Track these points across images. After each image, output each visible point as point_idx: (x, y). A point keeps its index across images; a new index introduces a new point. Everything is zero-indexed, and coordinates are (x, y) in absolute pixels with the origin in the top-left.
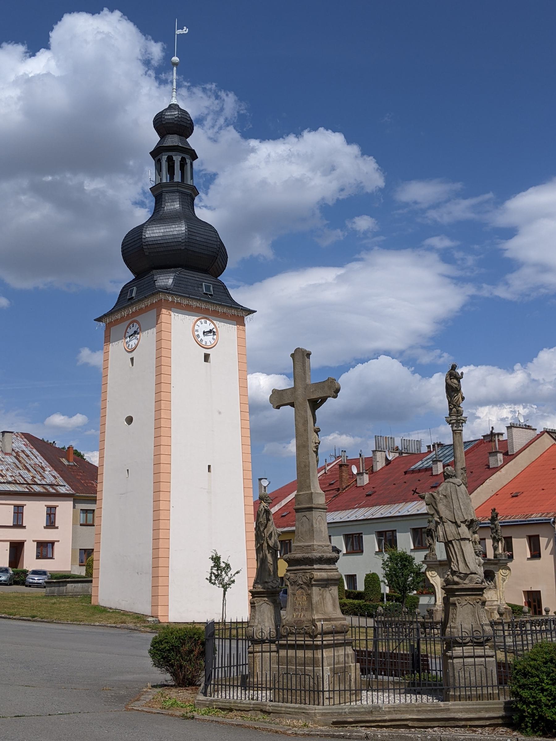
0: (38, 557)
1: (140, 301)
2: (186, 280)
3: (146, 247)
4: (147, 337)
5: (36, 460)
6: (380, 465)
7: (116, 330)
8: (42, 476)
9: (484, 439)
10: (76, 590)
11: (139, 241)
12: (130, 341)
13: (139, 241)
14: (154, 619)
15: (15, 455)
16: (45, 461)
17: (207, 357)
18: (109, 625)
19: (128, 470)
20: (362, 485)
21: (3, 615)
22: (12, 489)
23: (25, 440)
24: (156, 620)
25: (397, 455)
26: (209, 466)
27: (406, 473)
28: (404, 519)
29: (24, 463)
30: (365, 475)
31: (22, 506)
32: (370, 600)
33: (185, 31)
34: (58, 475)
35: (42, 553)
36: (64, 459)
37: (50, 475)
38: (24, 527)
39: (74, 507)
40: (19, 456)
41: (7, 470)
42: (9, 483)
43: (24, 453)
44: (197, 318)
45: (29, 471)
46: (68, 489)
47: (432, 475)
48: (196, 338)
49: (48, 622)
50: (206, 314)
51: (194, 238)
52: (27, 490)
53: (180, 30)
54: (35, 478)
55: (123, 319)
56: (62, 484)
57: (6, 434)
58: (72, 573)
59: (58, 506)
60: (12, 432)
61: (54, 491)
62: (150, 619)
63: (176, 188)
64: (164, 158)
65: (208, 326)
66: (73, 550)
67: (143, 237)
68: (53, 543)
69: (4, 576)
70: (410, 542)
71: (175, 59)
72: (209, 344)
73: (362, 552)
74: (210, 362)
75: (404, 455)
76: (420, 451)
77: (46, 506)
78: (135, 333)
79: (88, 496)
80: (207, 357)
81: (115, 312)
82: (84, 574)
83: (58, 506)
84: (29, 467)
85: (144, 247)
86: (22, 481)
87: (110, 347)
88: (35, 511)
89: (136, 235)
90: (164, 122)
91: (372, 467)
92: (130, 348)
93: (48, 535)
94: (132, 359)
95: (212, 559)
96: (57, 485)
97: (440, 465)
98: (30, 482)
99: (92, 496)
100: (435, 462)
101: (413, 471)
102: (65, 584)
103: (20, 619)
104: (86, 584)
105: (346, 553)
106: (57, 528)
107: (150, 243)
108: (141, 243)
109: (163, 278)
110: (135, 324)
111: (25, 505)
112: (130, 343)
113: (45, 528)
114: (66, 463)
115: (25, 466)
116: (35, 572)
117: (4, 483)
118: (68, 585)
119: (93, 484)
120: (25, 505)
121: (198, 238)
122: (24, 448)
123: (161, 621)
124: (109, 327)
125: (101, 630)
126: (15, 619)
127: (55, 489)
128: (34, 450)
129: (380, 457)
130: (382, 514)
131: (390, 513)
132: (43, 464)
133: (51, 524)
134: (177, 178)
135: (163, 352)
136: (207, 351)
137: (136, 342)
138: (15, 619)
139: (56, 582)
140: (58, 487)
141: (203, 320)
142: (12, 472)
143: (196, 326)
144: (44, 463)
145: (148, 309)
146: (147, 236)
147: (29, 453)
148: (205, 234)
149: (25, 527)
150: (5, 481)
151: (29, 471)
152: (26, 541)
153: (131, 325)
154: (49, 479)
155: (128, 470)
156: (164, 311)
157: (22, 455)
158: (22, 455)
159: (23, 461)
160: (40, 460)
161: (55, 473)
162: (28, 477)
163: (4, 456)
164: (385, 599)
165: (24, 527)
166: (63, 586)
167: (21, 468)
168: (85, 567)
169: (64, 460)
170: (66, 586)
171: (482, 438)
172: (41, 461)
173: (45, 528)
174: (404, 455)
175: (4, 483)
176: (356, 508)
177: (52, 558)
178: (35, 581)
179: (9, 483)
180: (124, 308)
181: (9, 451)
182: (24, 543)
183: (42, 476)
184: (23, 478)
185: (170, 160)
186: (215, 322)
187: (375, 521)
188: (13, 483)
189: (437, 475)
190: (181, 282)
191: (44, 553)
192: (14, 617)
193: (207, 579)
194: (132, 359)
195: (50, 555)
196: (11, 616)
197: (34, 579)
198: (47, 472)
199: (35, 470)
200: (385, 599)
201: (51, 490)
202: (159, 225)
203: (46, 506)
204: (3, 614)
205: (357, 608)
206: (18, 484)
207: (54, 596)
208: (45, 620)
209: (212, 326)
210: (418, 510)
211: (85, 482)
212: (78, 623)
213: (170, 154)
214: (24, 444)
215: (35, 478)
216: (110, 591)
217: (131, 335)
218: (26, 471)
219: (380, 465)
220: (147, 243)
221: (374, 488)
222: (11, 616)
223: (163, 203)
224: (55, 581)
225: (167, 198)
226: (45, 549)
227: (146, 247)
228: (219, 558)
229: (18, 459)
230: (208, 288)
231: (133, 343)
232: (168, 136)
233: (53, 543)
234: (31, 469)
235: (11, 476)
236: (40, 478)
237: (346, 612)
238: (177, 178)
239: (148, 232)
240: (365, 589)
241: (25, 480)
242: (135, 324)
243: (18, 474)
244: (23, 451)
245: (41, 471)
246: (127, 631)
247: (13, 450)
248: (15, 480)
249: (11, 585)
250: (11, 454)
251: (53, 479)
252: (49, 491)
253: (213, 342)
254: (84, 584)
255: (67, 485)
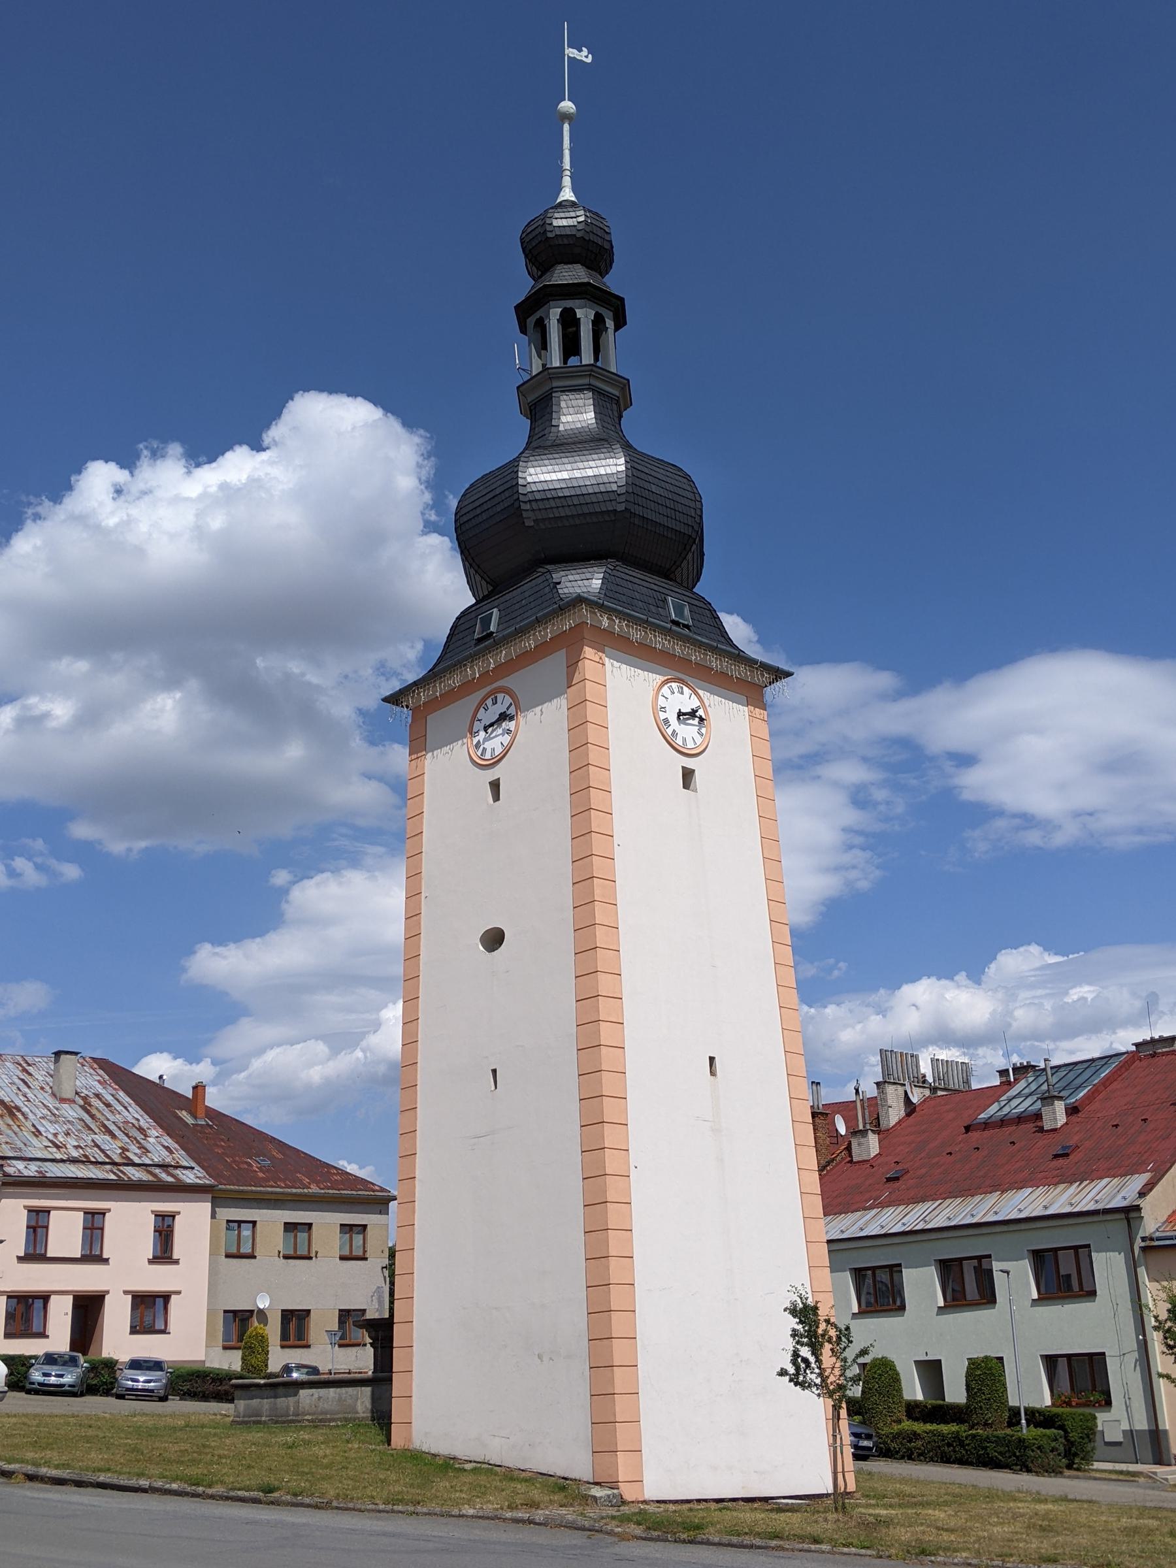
0: (134, 1331)
1: (506, 640)
2: (630, 585)
3: (528, 507)
4: (541, 728)
5: (126, 1113)
6: (894, 1114)
7: (434, 721)
8: (141, 1147)
9: (1138, 1051)
10: (323, 1406)
11: (507, 494)
12: (485, 740)
13: (507, 494)
14: (609, 1492)
15: (82, 1103)
16: (146, 1117)
17: (688, 776)
18: (509, 1515)
19: (494, 1071)
20: (866, 1158)
21: (174, 1486)
22: (80, 1175)
23: (101, 1072)
24: (614, 1496)
25: (927, 1093)
26: (712, 1059)
27: (968, 1129)
28: (1012, 1227)
29: (102, 1118)
30: (871, 1136)
31: (103, 1213)
32: (986, 1424)
33: (584, 56)
34: (176, 1146)
35: (142, 1322)
36: (184, 1113)
37: (159, 1146)
38: (106, 1261)
39: (213, 1216)
40: (90, 1105)
41: (67, 1134)
42: (74, 1161)
43: (100, 1100)
44: (663, 678)
45: (113, 1136)
46: (199, 1175)
47: (1041, 1130)
48: (662, 724)
49: (316, 1507)
50: (682, 670)
51: (646, 485)
52: (113, 1177)
53: (575, 51)
54: (128, 1150)
55: (467, 688)
56: (185, 1164)
57: (63, 1057)
58: (207, 1365)
59: (179, 1213)
60: (76, 1054)
61: (170, 1179)
62: (597, 1492)
63: (586, 381)
64: (554, 314)
65: (688, 701)
66: (211, 1313)
67: (521, 482)
68: (166, 1297)
69: (71, 1372)
70: (1029, 1284)
71: (567, 105)
72: (690, 745)
73: (994, 1302)
74: (695, 791)
75: (940, 1093)
76: (970, 1086)
77: (152, 1212)
78: (504, 717)
79: (242, 1191)
80: (688, 776)
81: (444, 670)
82: (237, 1366)
83: (179, 1213)
84: (113, 1128)
85: (523, 506)
86: (101, 1158)
87: (426, 762)
88: (129, 1222)
89: (499, 483)
90: (550, 235)
91: (878, 1118)
92: (488, 756)
93: (157, 1279)
94: (495, 786)
95: (793, 1311)
96: (176, 1167)
97: (1060, 1106)
98: (117, 1159)
99: (252, 1192)
100: (1048, 1099)
101: (986, 1125)
102: (291, 1390)
103: (227, 1498)
104: (350, 1390)
105: (860, 1313)
106: (177, 1262)
107: (538, 497)
108: (515, 497)
109: (577, 577)
110: (500, 696)
111: (109, 1210)
112: (488, 745)
113: (150, 1262)
114: (190, 1120)
115: (105, 1126)
116: (136, 1365)
117: (62, 1161)
118: (302, 1392)
119: (250, 1165)
120: (109, 1210)
121: (654, 488)
122: (100, 1089)
123: (628, 1497)
124: (420, 715)
125: (479, 1532)
126: (212, 1497)
127: (173, 1176)
128: (121, 1093)
129: (894, 1095)
130: (949, 1218)
131: (973, 1216)
132: (142, 1123)
133: (164, 1253)
134: (587, 357)
135: (591, 755)
136: (690, 763)
137: (506, 739)
138: (212, 1497)
139: (265, 1385)
140: (178, 1172)
141: (674, 685)
142: (79, 1138)
143: (660, 698)
144: (145, 1121)
145: (544, 650)
146: (529, 479)
147: (110, 1099)
148: (669, 480)
149: (106, 1261)
150: (65, 1157)
151: (113, 1136)
152: (108, 1292)
153: (489, 702)
154: (158, 1154)
155: (494, 1071)
156: (588, 652)
157: (95, 1102)
158: (95, 1102)
159: (98, 1115)
160: (135, 1114)
161: (168, 1141)
162: (113, 1148)
163: (58, 1105)
164: (1023, 1421)
165: (106, 1261)
166: (286, 1397)
167: (97, 1130)
168: (239, 1353)
169: (184, 1115)
170: (296, 1394)
171: (1134, 1048)
172: (136, 1116)
173: (150, 1262)
174: (940, 1093)
175: (62, 1161)
176: (871, 1208)
177: (164, 1332)
178: (140, 1385)
179: (74, 1161)
180: (473, 658)
181: (69, 1094)
182: (103, 1297)
183: (141, 1147)
184: (102, 1151)
185: (569, 322)
186: (700, 692)
187: (934, 1236)
188: (83, 1162)
189: (1055, 1130)
190: (620, 589)
191: (148, 1320)
192: (210, 1491)
193: (783, 1373)
194: (495, 786)
195: (159, 1325)
196: (200, 1489)
197: (137, 1381)
198: (151, 1140)
199: (127, 1135)
200: (1023, 1421)
201: (164, 1176)
202: (556, 456)
203: (152, 1212)
204: (174, 1480)
205: (949, 1445)
206: (92, 1163)
207: (259, 1422)
208: (307, 1500)
209: (694, 703)
210: (842, 1232)
211: (234, 1161)
212: (411, 1508)
213: (569, 304)
214: (99, 1081)
215: (128, 1150)
216: (441, 1408)
217: (492, 725)
218: (108, 1138)
219: (894, 1114)
220: (531, 497)
221: (897, 1163)
222: (200, 1489)
223: (554, 415)
224: (262, 1381)
225: (563, 404)
226: (149, 1309)
227: (528, 507)
228: (815, 1309)
229: (88, 1112)
230: (679, 610)
231: (496, 743)
232: (559, 267)
233: (166, 1297)
234: (117, 1133)
235: (76, 1147)
236: (138, 1151)
237: (920, 1455)
238: (587, 357)
239: (532, 470)
240: (968, 1397)
241: (107, 1156)
242: (500, 696)
243: (90, 1143)
244: (98, 1096)
245: (140, 1137)
246: (578, 1538)
247: (77, 1093)
248: (85, 1156)
249: (82, 1395)
250: (74, 1102)
251: (165, 1153)
252: (160, 1180)
253: (699, 740)
254: (343, 1390)
255: (197, 1168)
